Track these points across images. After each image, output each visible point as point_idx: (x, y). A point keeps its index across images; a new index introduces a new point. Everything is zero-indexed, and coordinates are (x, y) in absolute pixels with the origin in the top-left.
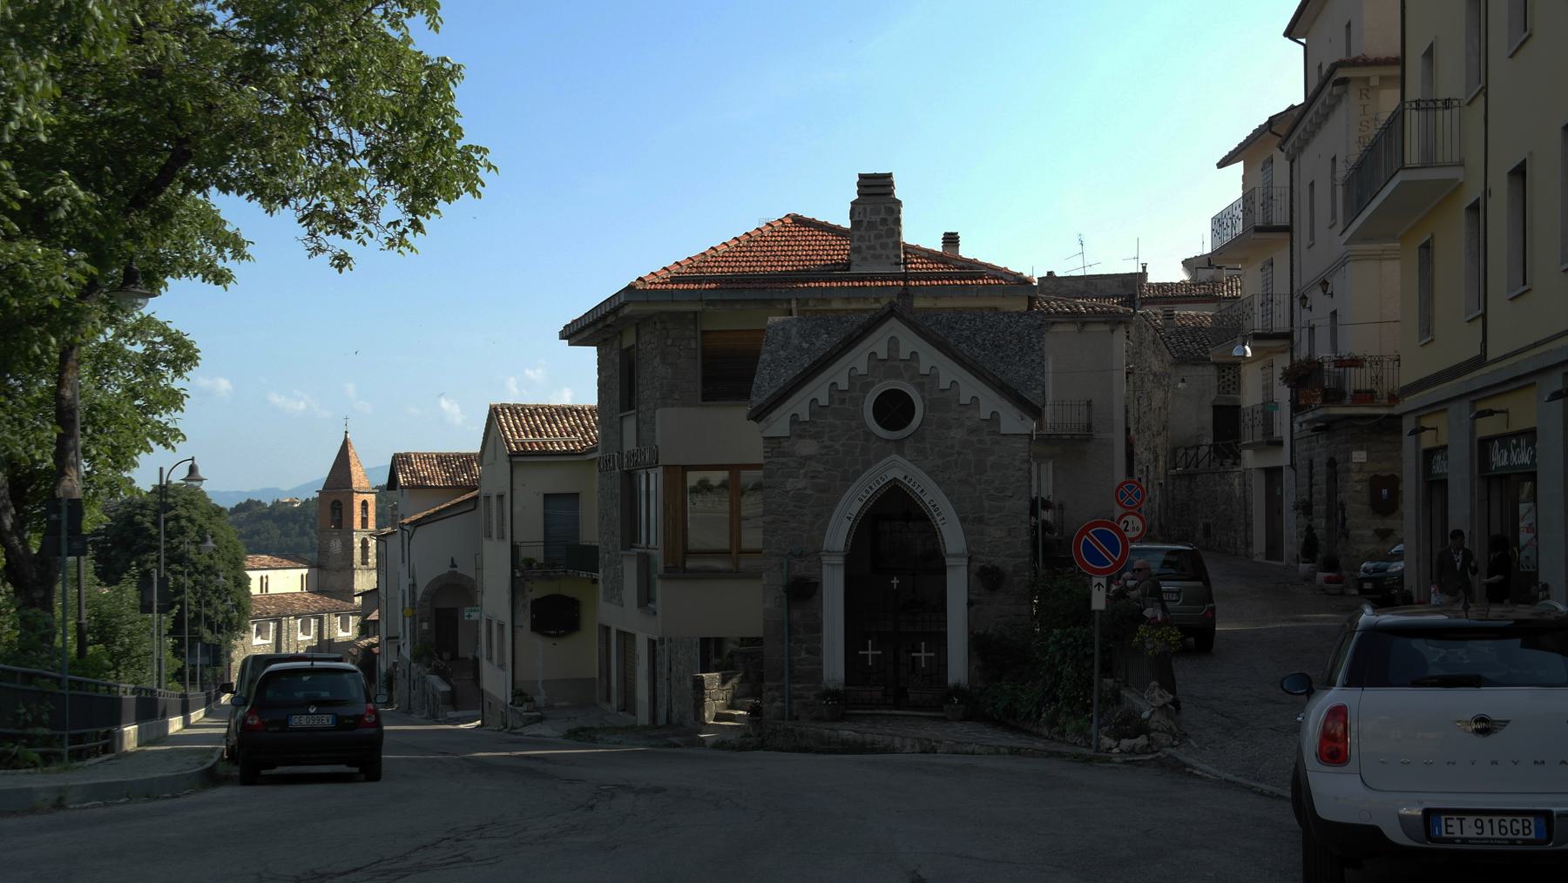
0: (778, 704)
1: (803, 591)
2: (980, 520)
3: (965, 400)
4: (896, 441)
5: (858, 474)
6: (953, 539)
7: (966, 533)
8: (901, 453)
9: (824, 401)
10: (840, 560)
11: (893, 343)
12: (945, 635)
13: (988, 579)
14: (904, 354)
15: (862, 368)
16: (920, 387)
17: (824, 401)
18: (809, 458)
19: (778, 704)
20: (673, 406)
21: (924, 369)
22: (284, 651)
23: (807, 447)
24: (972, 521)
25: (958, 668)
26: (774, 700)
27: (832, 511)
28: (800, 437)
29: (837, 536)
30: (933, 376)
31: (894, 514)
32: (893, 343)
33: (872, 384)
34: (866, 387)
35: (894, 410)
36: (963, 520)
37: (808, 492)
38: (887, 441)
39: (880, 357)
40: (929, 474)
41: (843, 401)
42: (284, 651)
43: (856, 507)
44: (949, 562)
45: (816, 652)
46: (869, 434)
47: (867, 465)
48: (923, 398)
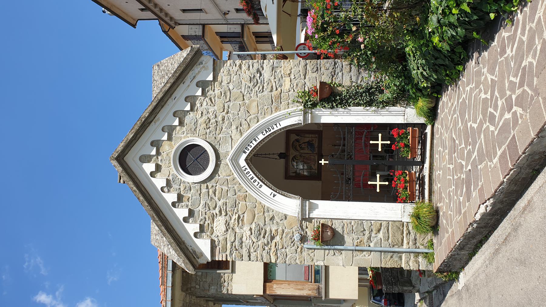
29: (289, 205)
43: (266, 190)
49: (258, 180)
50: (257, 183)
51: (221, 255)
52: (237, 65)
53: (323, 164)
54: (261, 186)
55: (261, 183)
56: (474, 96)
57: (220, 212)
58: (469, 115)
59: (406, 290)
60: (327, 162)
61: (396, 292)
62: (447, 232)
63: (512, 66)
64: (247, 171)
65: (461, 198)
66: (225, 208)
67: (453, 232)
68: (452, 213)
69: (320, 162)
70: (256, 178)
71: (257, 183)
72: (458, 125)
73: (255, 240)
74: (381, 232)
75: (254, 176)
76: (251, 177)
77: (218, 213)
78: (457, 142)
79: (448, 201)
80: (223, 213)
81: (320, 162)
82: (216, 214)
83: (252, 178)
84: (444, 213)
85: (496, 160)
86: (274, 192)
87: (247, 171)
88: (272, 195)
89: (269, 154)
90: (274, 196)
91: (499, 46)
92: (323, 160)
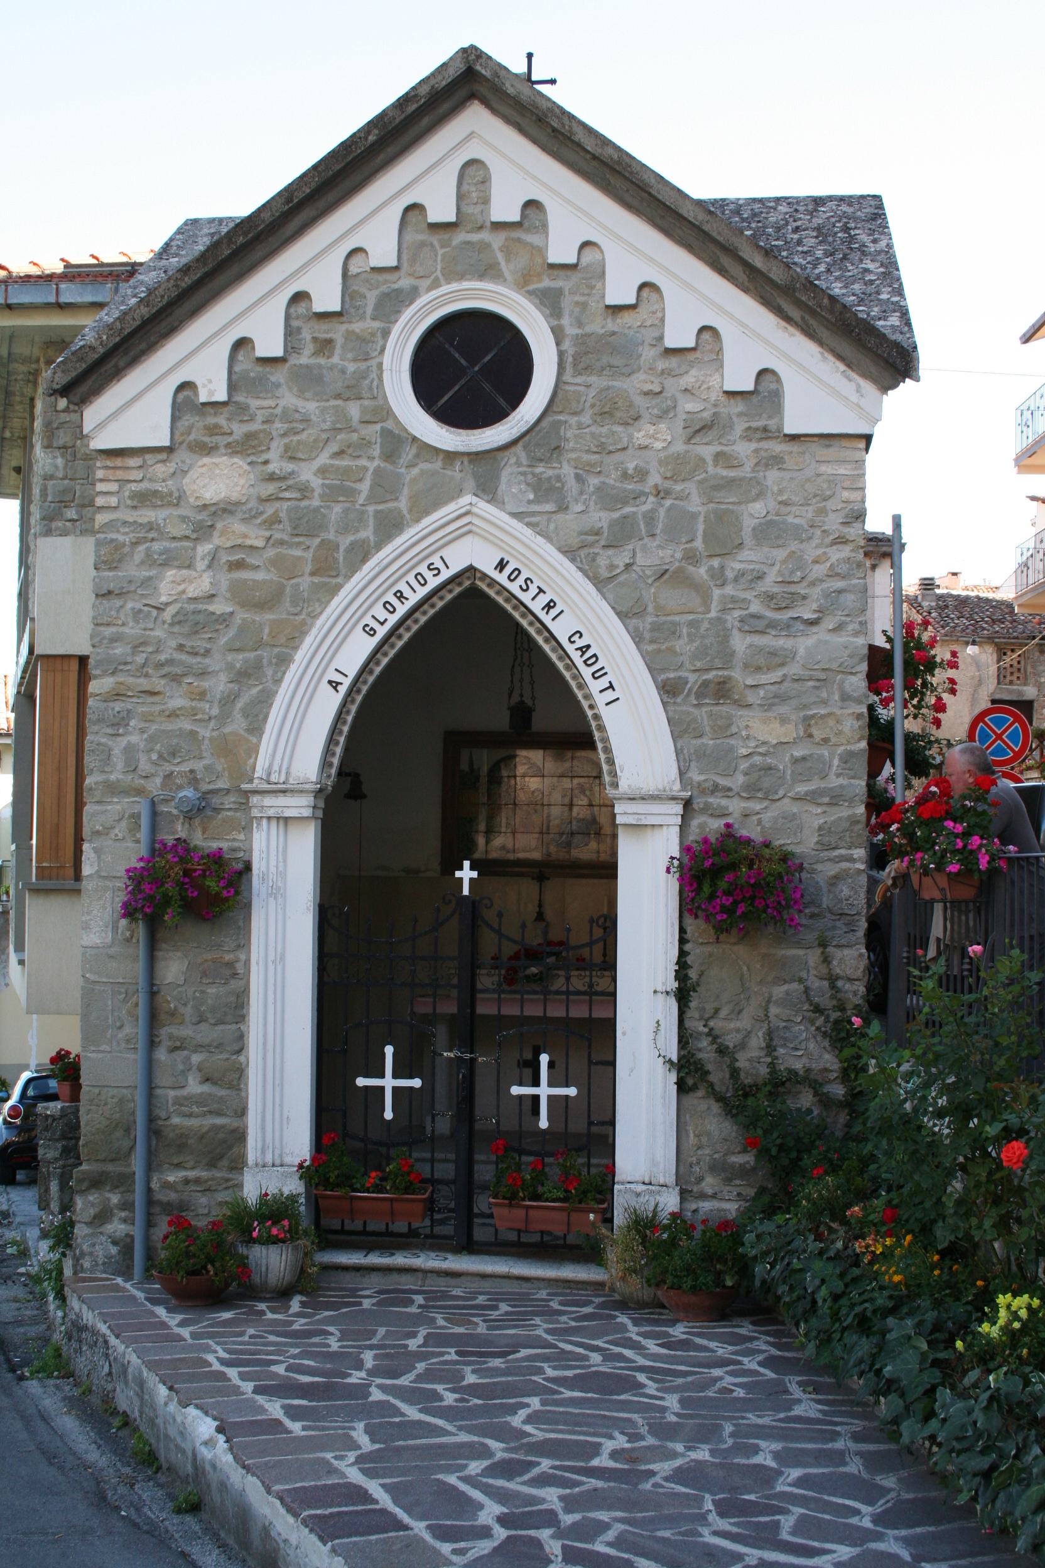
0: (117, 1227)
1: (189, 892)
2: (721, 691)
3: (680, 335)
4: (476, 457)
5: (361, 554)
6: (638, 741)
7: (679, 728)
8: (488, 489)
9: (270, 344)
10: (301, 805)
11: (473, 175)
12: (610, 1025)
13: (730, 887)
14: (505, 206)
15: (383, 249)
16: (550, 302)
17: (270, 344)
18: (226, 509)
19: (117, 1227)
20: (64, 533)
21: (561, 250)
22: (479, 996)
23: (218, 479)
24: (696, 695)
25: (648, 1138)
26: (102, 1217)
27: (284, 661)
28: (205, 449)
29: (299, 736)
30: (586, 268)
31: (467, 703)
32: (473, 175)
33: (407, 297)
34: (393, 303)
35: (471, 368)
36: (669, 690)
37: (219, 607)
38: (450, 457)
39: (433, 217)
40: (570, 553)
41: (324, 346)
42: (479, 996)
43: (356, 651)
44: (624, 813)
45: (231, 1077)
46: (397, 441)
47: (390, 526)
48: (558, 334)
49: (393, 619)
50: (382, 614)
51: (114, 487)
52: (846, 530)
53: (458, 874)
54: (372, 632)
55: (382, 631)
56: (629, 1420)
57: (272, 478)
58: (572, 1402)
59: (47, 1190)
60: (466, 891)
61: (41, 1152)
62: (181, 1324)
63: (660, 1534)
64: (428, 575)
65: (280, 1369)
66: (287, 495)
67: (180, 1338)
68: (246, 1338)
69: (467, 864)
70: (402, 610)
71: (382, 614)
72: (555, 1368)
73: (168, 615)
74: (206, 1088)
75: (408, 605)
76: (407, 592)
77: (271, 468)
78: (497, 1362)
79: (295, 1327)
80: (271, 488)
81: (467, 864)
82: (266, 462)
83: (400, 596)
84: (263, 1313)
85: (355, 1476)
86: (347, 683)
87: (428, 575)
88: (338, 678)
89: (532, 683)
90: (334, 685)
91: (768, 1497)
92: (475, 874)
